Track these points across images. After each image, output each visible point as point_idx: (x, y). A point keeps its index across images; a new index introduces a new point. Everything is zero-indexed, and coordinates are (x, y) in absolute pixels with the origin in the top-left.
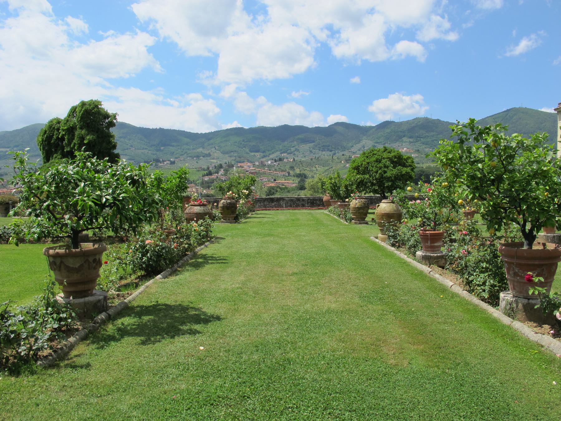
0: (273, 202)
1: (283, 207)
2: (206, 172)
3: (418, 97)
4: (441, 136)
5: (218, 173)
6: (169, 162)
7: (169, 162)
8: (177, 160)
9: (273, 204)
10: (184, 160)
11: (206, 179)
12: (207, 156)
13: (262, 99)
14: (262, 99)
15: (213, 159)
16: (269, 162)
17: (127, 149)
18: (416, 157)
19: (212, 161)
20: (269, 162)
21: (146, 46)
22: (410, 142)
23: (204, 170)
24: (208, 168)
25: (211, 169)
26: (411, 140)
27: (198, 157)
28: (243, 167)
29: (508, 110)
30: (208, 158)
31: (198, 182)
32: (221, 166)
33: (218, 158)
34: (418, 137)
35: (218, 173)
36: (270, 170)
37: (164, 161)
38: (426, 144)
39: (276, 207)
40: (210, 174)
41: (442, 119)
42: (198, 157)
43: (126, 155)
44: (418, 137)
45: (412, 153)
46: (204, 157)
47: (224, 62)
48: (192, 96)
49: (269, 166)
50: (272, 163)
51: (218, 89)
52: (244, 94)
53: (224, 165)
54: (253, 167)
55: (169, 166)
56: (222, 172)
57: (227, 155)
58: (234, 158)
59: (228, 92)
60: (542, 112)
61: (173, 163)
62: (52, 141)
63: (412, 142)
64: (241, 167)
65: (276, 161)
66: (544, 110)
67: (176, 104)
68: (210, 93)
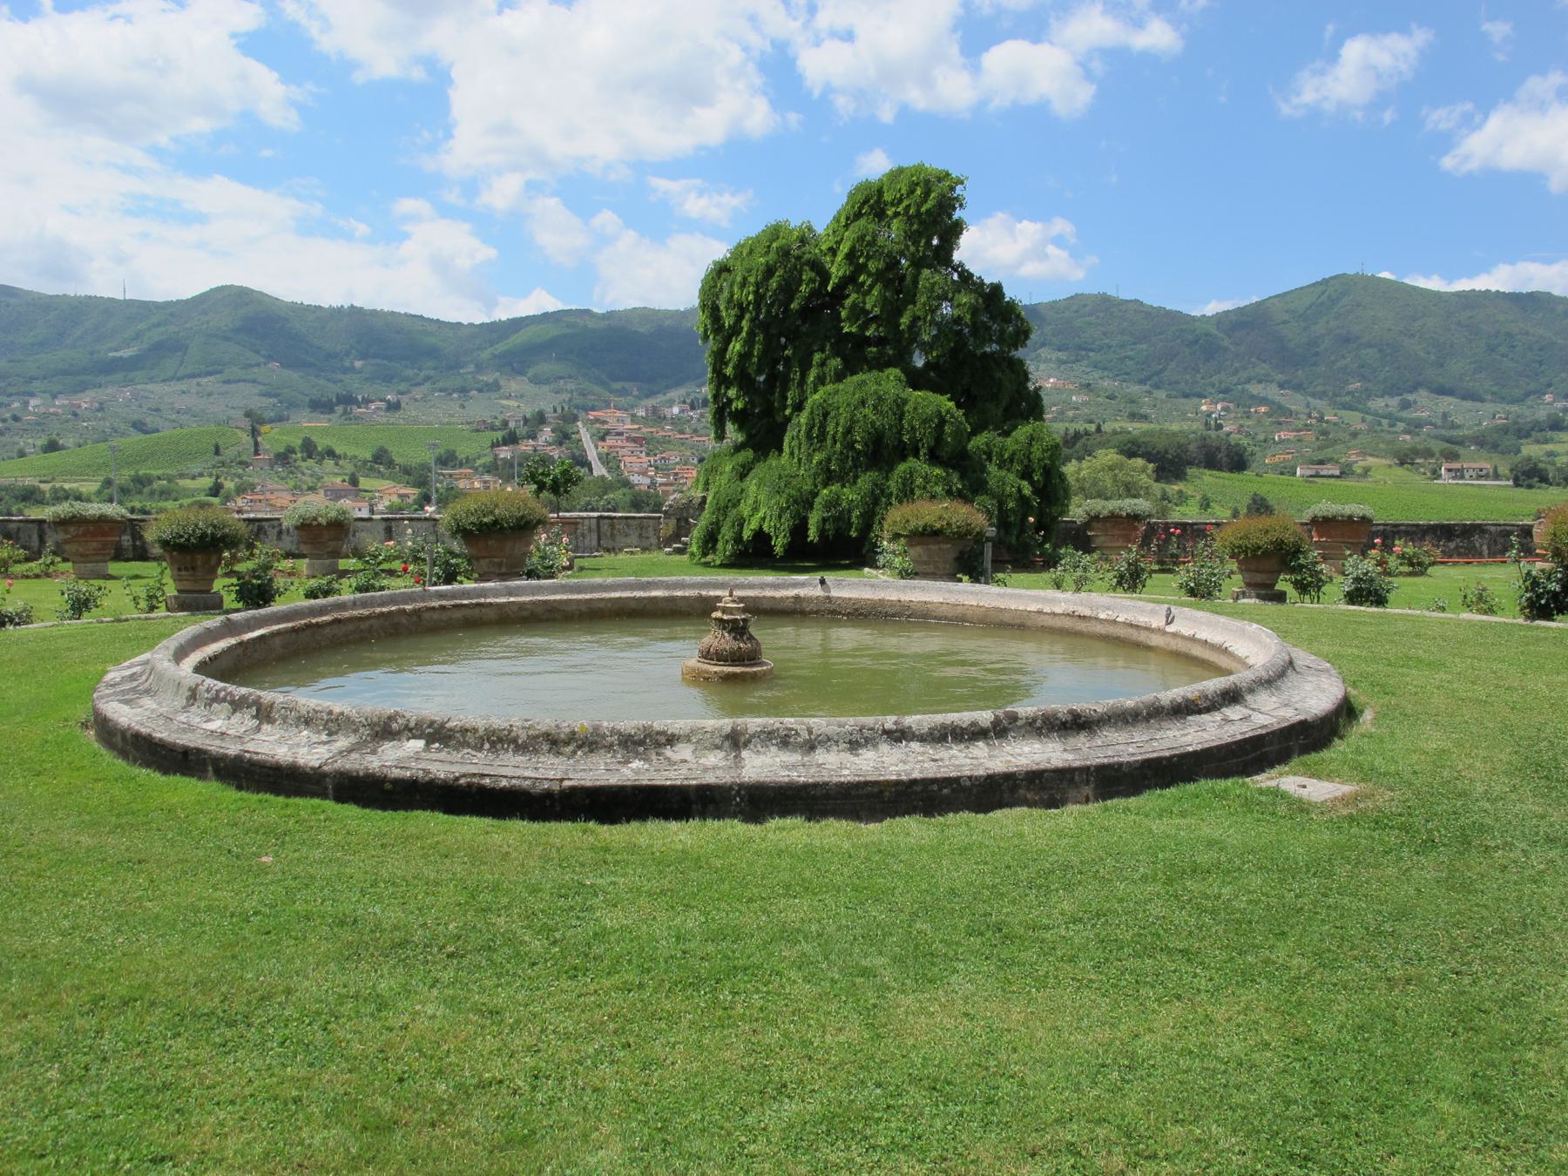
0: (1449, 539)
1: (1481, 555)
2: (499, 435)
3: (1061, 226)
4: (1144, 346)
5: (534, 438)
6: (383, 405)
7: (383, 405)
8: (404, 399)
9: (1452, 545)
10: (424, 399)
11: (505, 453)
12: (490, 390)
13: (607, 219)
14: (607, 219)
15: (509, 397)
16: (676, 410)
17: (258, 365)
18: (1085, 404)
19: (505, 402)
20: (676, 410)
21: (234, 36)
22: (1061, 362)
23: (493, 428)
24: (505, 423)
25: (512, 425)
26: (1063, 355)
27: (463, 390)
28: (605, 422)
29: (1325, 282)
30: (493, 395)
31: (479, 462)
32: (541, 419)
33: (518, 399)
34: (1080, 348)
35: (534, 438)
36: (682, 432)
37: (367, 401)
38: (1105, 369)
39: (1460, 555)
40: (511, 439)
41: (1147, 301)
42: (463, 390)
43: (254, 381)
44: (1080, 348)
45: (1071, 392)
46: (480, 391)
47: (469, 101)
48: (408, 205)
49: (675, 421)
50: (682, 411)
51: (471, 187)
52: (553, 202)
53: (550, 415)
54: (633, 422)
55: (383, 417)
56: (547, 433)
57: (546, 388)
58: (566, 396)
59: (503, 194)
60: (1415, 288)
61: (394, 407)
62: (794, 306)
63: (1064, 362)
64: (597, 420)
65: (693, 408)
66: (1422, 283)
67: (362, 229)
68: (453, 197)
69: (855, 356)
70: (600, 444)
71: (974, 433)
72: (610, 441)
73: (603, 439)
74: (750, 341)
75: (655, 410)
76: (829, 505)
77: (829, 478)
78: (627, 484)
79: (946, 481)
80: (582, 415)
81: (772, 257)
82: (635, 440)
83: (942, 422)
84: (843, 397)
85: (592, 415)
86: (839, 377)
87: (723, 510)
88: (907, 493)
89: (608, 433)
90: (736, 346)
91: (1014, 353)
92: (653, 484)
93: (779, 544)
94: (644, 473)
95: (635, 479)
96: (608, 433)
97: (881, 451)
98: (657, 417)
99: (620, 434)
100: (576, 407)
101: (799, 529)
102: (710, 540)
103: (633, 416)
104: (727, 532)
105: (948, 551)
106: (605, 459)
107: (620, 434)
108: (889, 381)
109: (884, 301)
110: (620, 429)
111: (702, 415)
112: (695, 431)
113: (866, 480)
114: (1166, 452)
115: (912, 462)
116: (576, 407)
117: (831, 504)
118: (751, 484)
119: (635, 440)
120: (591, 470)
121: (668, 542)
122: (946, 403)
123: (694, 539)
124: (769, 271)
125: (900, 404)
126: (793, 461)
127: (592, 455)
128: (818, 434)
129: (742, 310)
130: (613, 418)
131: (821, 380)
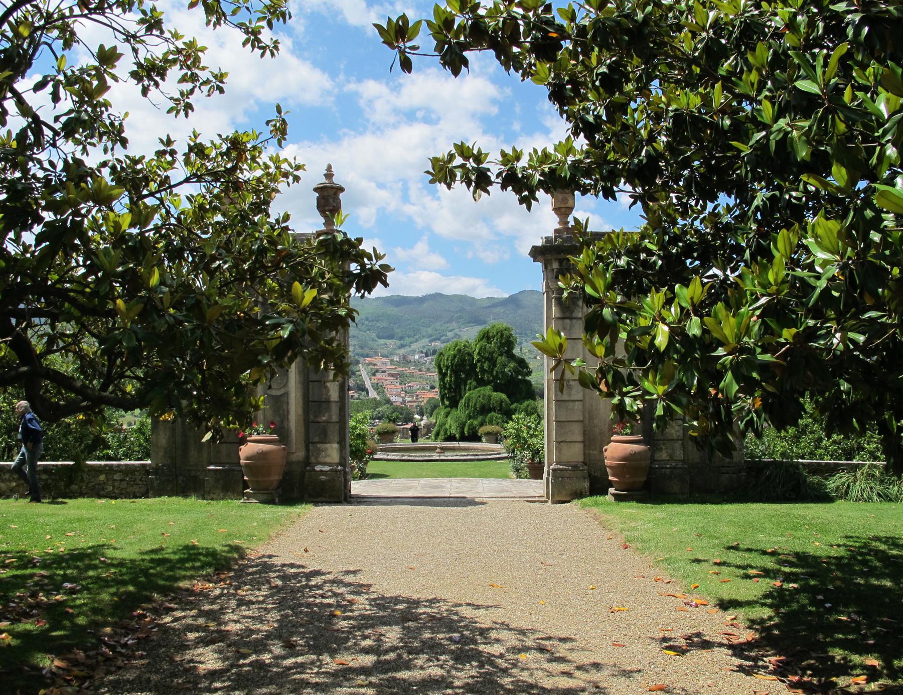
16: (417, 357)
20: (417, 357)
28: (375, 365)
36: (420, 370)
49: (416, 363)
64: (370, 364)
65: (427, 355)
69: (481, 383)
70: (373, 377)
71: (512, 403)
72: (379, 376)
73: (374, 375)
74: (451, 377)
75: (404, 357)
76: (469, 425)
77: (470, 418)
78: (388, 401)
79: (502, 418)
80: (361, 359)
81: (455, 352)
82: (393, 375)
83: (502, 402)
84: (474, 394)
85: (368, 360)
86: (475, 387)
87: (441, 426)
88: (491, 423)
89: (377, 371)
90: (448, 379)
91: (527, 378)
92: (404, 401)
93: (457, 436)
94: (398, 395)
95: (393, 399)
96: (377, 371)
97: (485, 410)
98: (405, 361)
99: (384, 372)
100: (357, 354)
101: (462, 433)
102: (437, 435)
103: (392, 360)
104: (442, 432)
105: (494, 437)
106: (376, 387)
107: (384, 372)
108: (487, 390)
109: (489, 367)
110: (384, 369)
111: (432, 360)
112: (428, 369)
113: (480, 419)
114: (31, 500)
115: (493, 413)
116: (357, 354)
117: (471, 424)
118: (449, 419)
119: (393, 375)
120: (368, 393)
121: (424, 436)
122: (504, 396)
123: (432, 435)
124: (455, 356)
125: (490, 396)
126: (460, 413)
127: (368, 385)
128: (467, 406)
129: (447, 368)
130: (380, 362)
131: (470, 389)
